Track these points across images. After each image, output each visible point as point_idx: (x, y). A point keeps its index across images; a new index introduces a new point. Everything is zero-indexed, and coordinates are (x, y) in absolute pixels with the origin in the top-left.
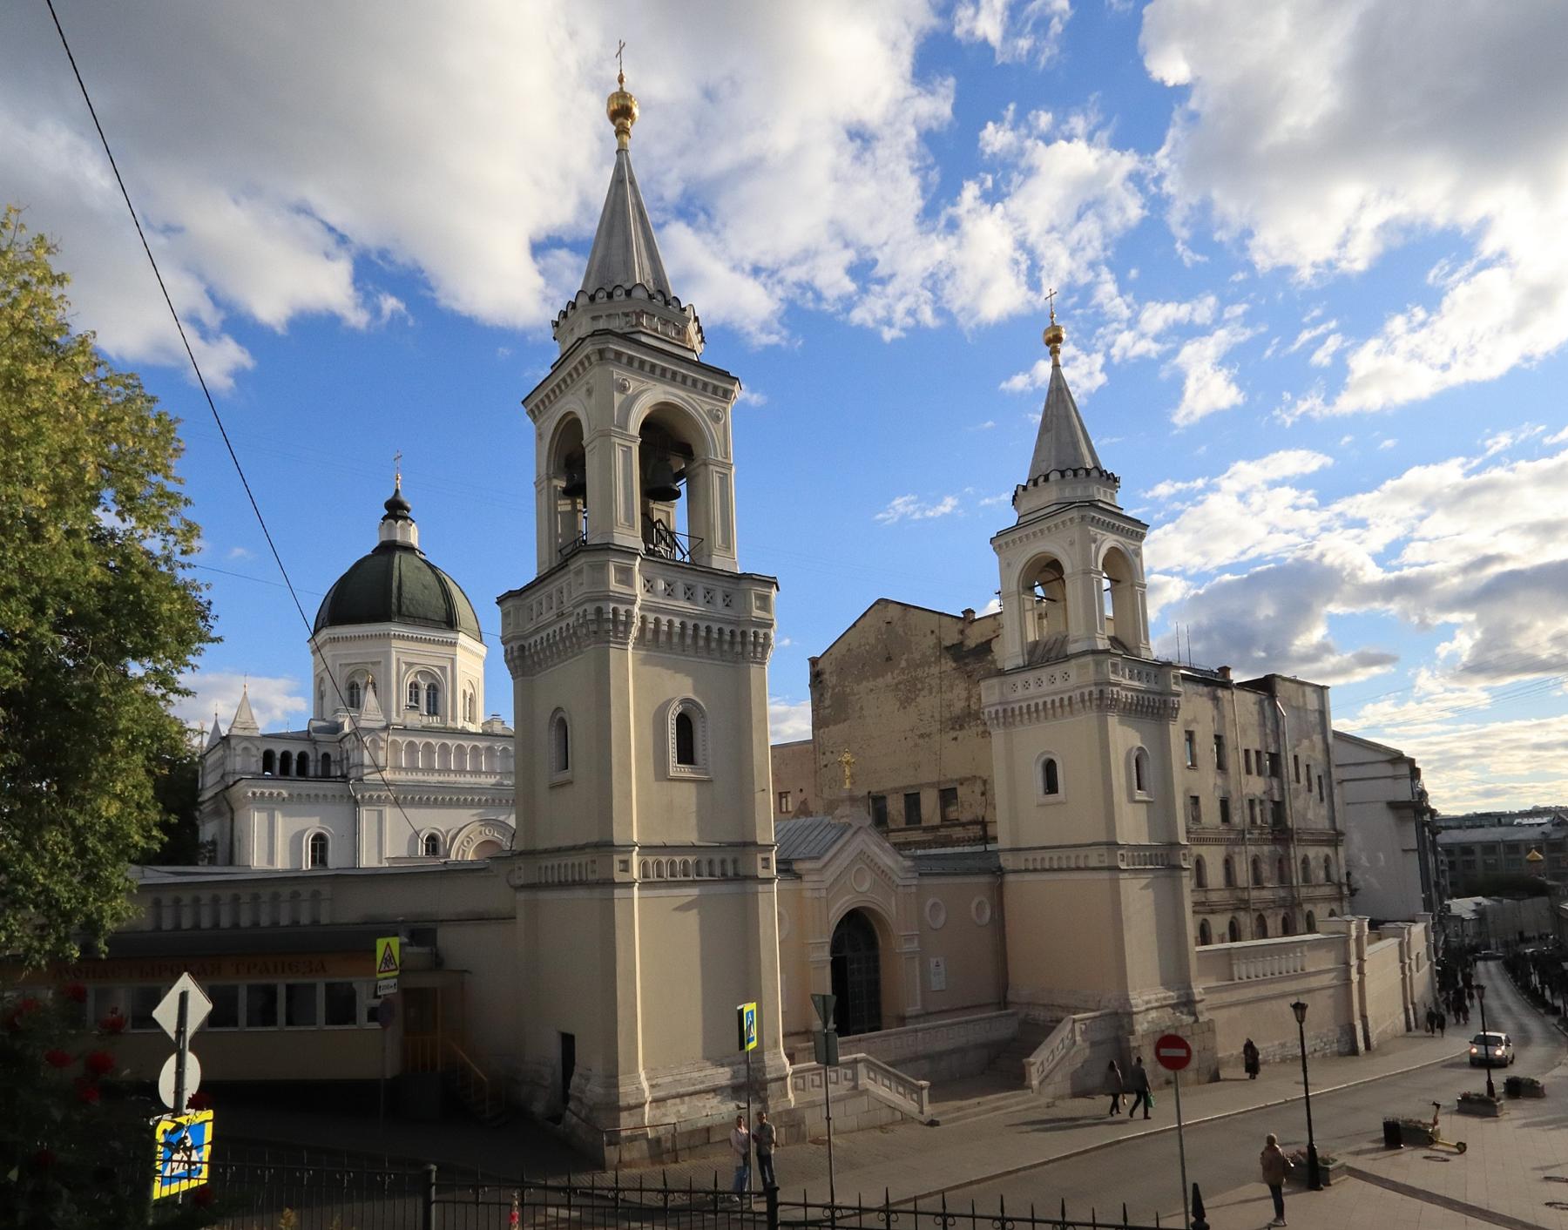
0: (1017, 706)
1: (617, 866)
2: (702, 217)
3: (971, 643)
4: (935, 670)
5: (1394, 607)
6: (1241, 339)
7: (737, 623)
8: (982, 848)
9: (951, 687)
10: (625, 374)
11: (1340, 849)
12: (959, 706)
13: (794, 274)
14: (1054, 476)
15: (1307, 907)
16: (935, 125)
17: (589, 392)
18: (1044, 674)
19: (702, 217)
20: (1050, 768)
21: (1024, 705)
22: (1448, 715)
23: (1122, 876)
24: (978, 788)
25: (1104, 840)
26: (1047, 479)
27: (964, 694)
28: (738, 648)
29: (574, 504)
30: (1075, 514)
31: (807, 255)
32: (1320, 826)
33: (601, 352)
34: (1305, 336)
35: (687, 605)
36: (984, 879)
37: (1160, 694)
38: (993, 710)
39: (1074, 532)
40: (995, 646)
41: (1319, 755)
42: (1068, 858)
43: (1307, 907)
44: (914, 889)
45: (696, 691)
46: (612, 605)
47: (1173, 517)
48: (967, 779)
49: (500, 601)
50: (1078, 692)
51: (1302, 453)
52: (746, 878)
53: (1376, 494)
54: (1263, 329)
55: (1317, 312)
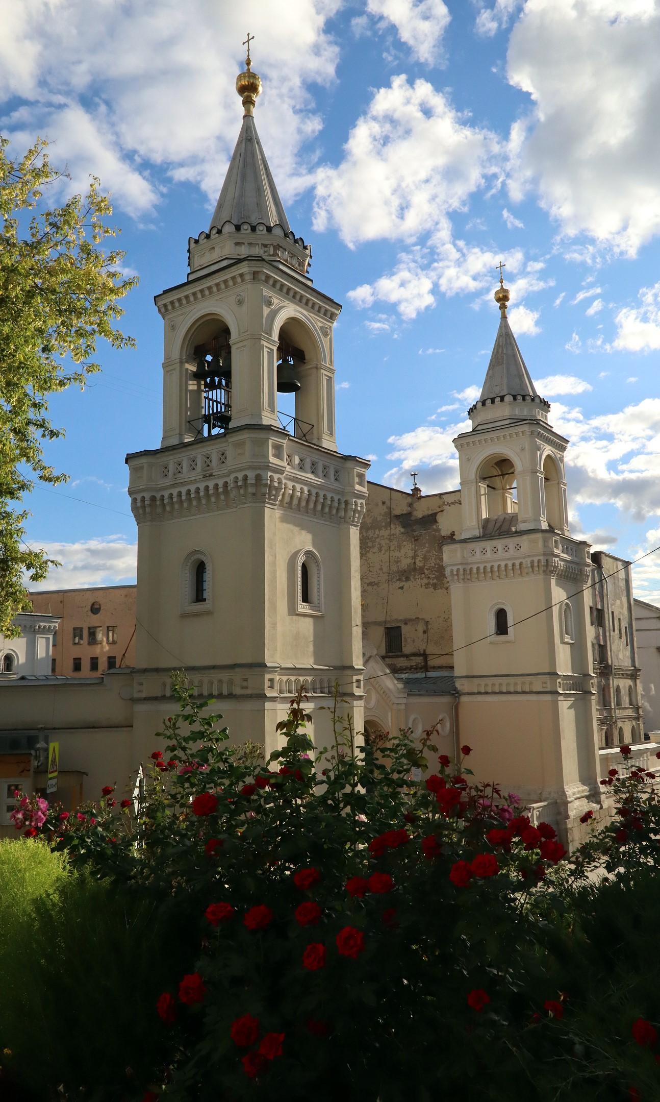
0: (475, 567)
1: (267, 684)
2: (103, 108)
3: (419, 514)
4: (385, 533)
5: (619, 503)
6: (536, 288)
7: (342, 493)
8: (423, 675)
9: (399, 547)
10: (271, 294)
11: (638, 681)
12: (405, 563)
13: (181, 174)
14: (508, 398)
15: (620, 724)
16: (319, 80)
17: (240, 303)
18: (488, 545)
19: (103, 108)
20: (501, 616)
22: (646, 584)
23: (561, 698)
24: (421, 627)
25: (547, 671)
26: (502, 399)
27: (411, 554)
28: (342, 513)
29: (199, 385)
30: (526, 428)
31: (194, 160)
32: (626, 664)
33: (255, 274)
34: (581, 296)
35: (312, 476)
36: (445, 700)
37: (577, 564)
38: (455, 569)
40: (439, 518)
41: (625, 611)
42: (500, 685)
43: (620, 724)
44: (403, 707)
45: (314, 546)
46: (270, 474)
48: (411, 620)
49: (129, 458)
50: (529, 560)
51: (572, 379)
52: (345, 694)
53: (620, 416)
54: (552, 283)
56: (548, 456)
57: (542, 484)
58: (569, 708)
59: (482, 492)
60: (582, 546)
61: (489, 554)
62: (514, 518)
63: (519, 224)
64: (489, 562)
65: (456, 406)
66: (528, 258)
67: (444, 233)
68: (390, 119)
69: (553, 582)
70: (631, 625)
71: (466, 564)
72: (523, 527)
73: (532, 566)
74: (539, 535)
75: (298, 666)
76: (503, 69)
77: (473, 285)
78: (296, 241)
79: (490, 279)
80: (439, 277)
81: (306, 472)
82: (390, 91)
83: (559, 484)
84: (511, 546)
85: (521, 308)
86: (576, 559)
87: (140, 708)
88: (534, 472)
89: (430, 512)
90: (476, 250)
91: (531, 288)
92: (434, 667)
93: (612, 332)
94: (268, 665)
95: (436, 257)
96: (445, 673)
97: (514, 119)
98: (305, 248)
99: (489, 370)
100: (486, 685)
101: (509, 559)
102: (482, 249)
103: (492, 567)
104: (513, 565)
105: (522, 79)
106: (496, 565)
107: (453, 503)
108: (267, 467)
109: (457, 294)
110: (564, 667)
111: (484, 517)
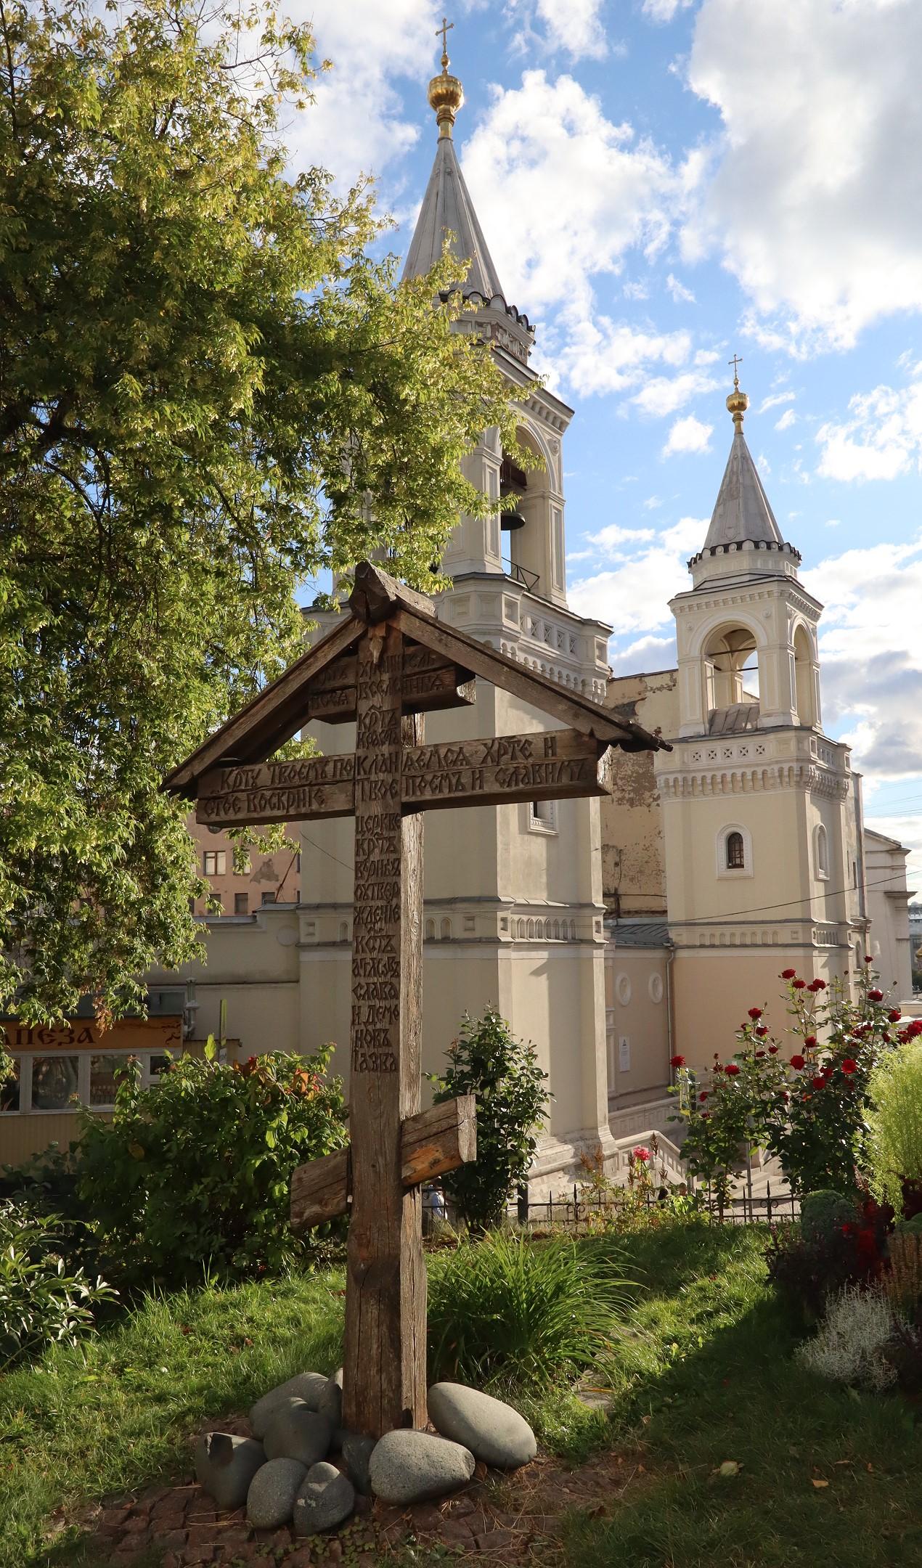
0: (699, 776)
1: (500, 924)
6: (705, 389)
14: (748, 546)
16: (410, 72)
18: (719, 746)
20: (734, 841)
21: (709, 775)
23: (816, 953)
25: (799, 916)
26: (739, 545)
30: (774, 587)
35: (544, 645)
36: (658, 954)
39: (772, 606)
42: (733, 935)
46: (502, 641)
47: (614, 567)
50: (776, 767)
52: (582, 941)
55: (781, 380)
56: (800, 627)
57: (792, 665)
58: (823, 966)
59: (709, 674)
60: (839, 750)
61: (720, 759)
62: (751, 712)
63: (689, 296)
64: (718, 769)
65: (587, 554)
66: (697, 345)
67: (581, 304)
68: (517, 136)
69: (808, 797)
70: (860, 859)
71: (688, 772)
72: (766, 722)
73: (781, 776)
74: (792, 734)
75: (532, 902)
76: (684, 68)
77: (618, 382)
78: (519, 319)
79: (642, 372)
80: (571, 368)
81: (539, 640)
82: (518, 94)
83: (810, 664)
84: (751, 749)
85: (691, 419)
86: (833, 768)
87: (308, 957)
88: (784, 647)
89: (626, 701)
90: (626, 331)
91: (698, 390)
92: (629, 912)
93: (813, 456)
94: (503, 899)
95: (568, 340)
96: (658, 920)
97: (693, 146)
98: (530, 329)
99: (718, 505)
100: (733, 935)
101: (747, 766)
102: (634, 330)
103: (723, 776)
104: (754, 773)
105: (708, 85)
106: (729, 773)
107: (659, 689)
108: (500, 632)
109: (595, 392)
110: (819, 914)
111: (710, 708)
